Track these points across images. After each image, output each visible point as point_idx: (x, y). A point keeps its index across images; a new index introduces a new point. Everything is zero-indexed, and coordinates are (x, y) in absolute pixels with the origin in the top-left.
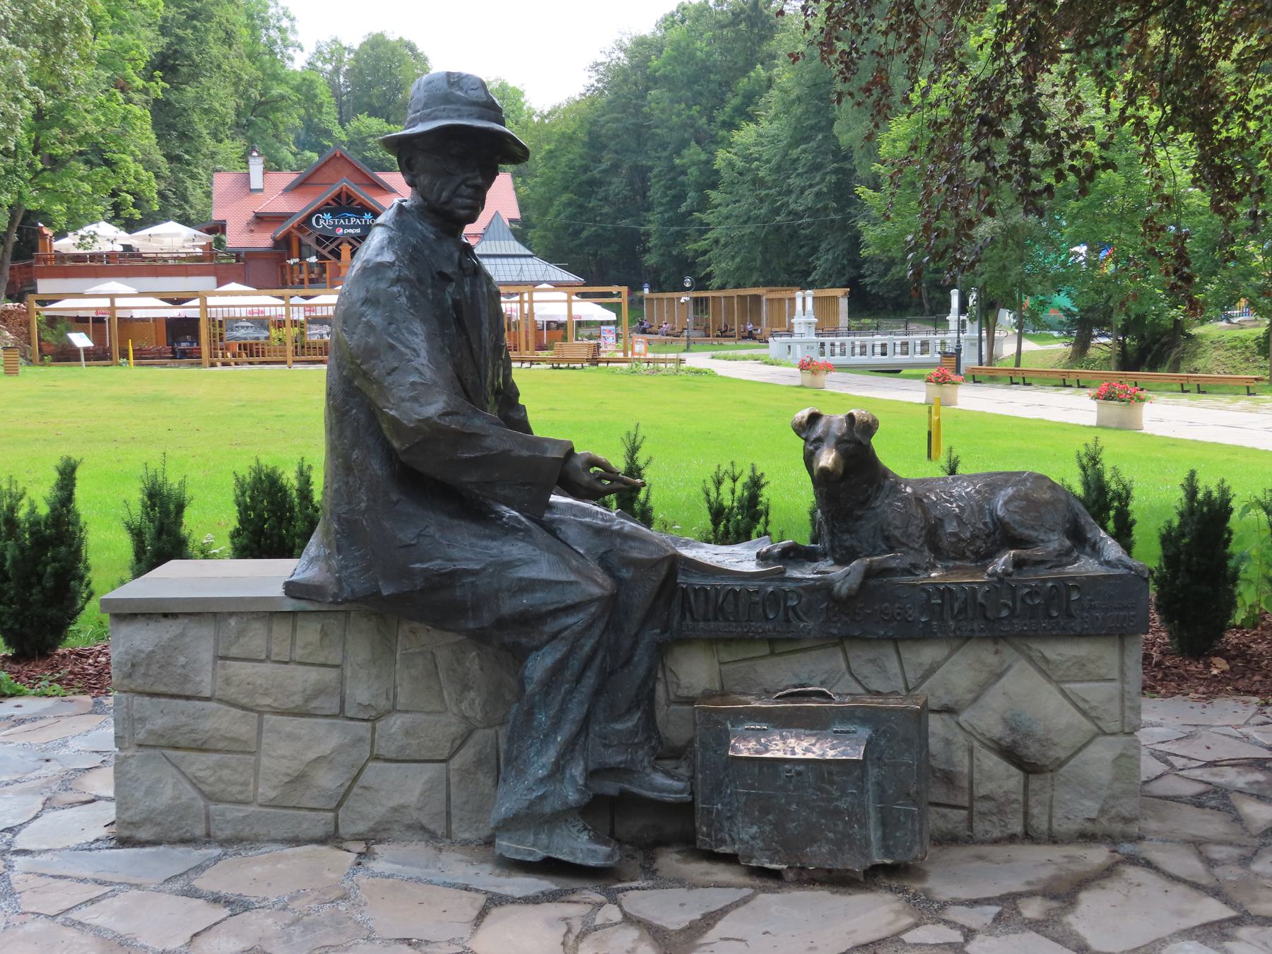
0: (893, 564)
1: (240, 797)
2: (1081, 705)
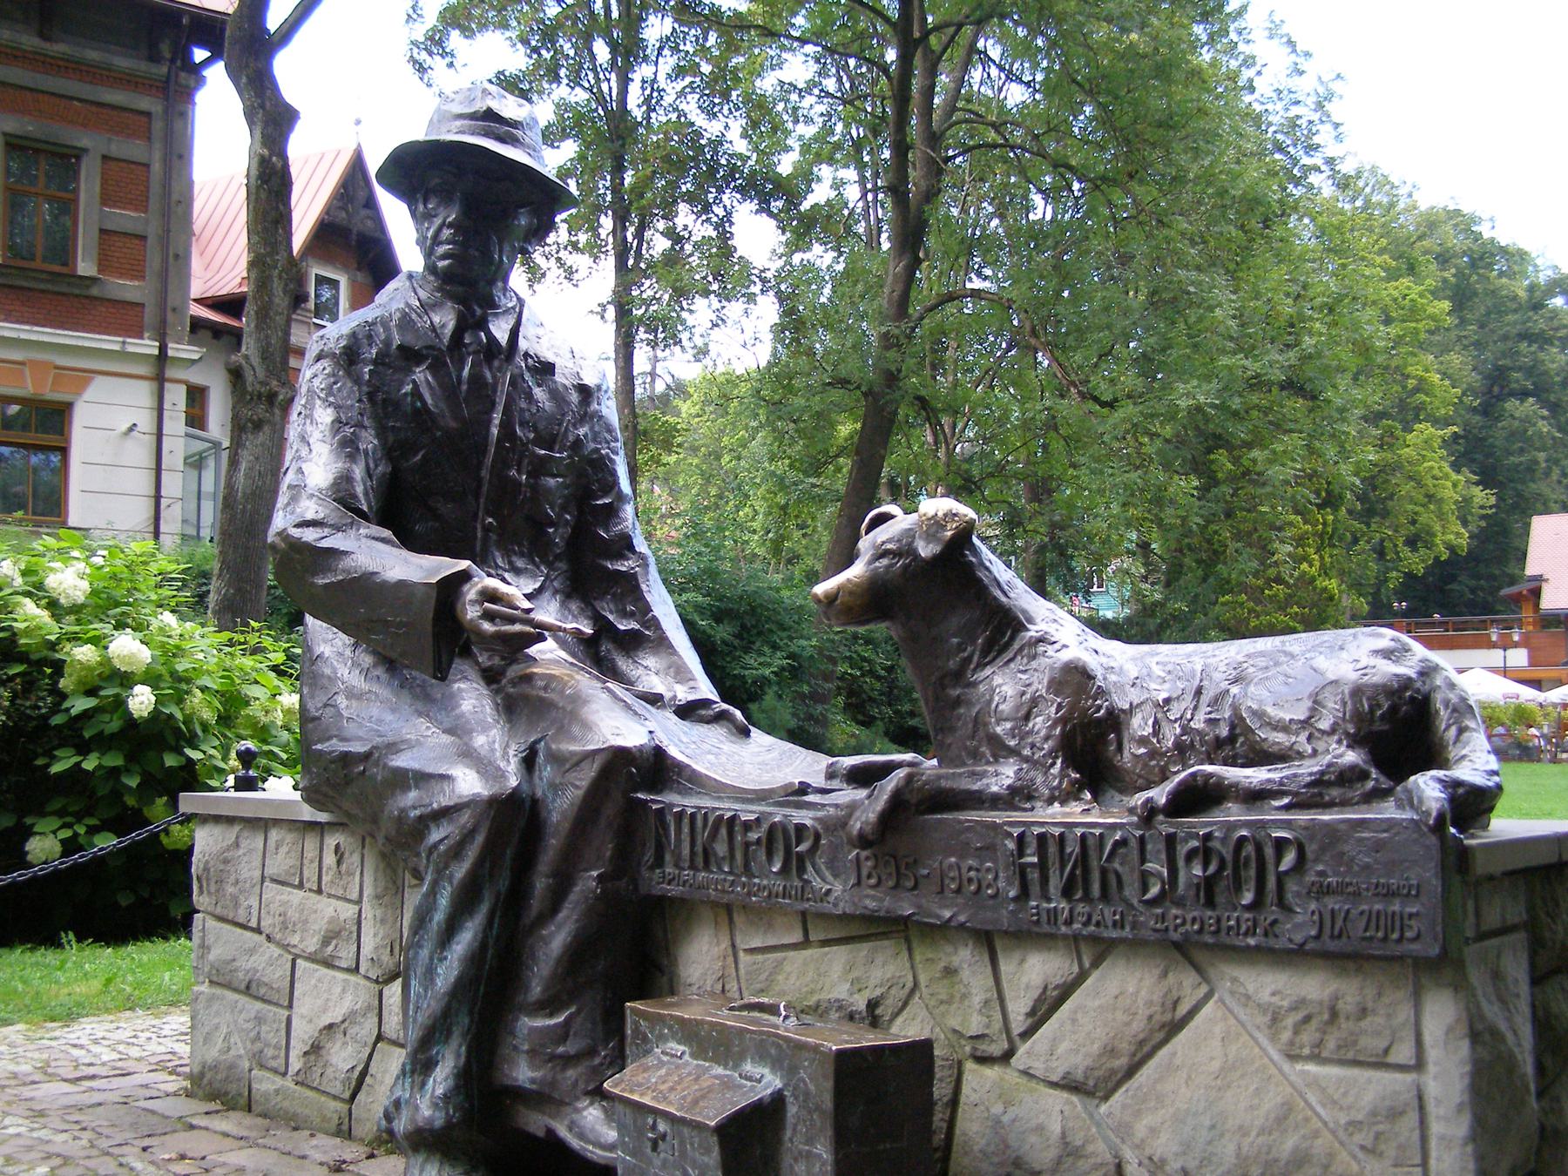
1: (273, 1064)
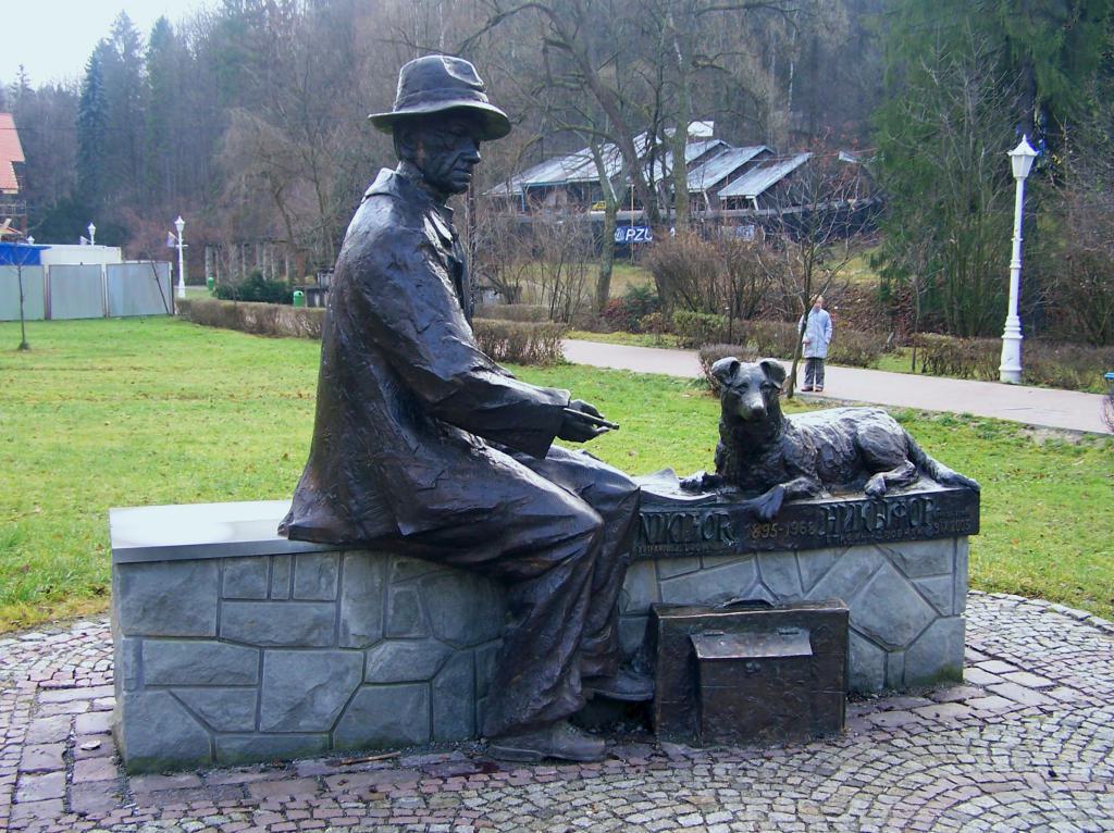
0: (798, 489)
2: (926, 594)
